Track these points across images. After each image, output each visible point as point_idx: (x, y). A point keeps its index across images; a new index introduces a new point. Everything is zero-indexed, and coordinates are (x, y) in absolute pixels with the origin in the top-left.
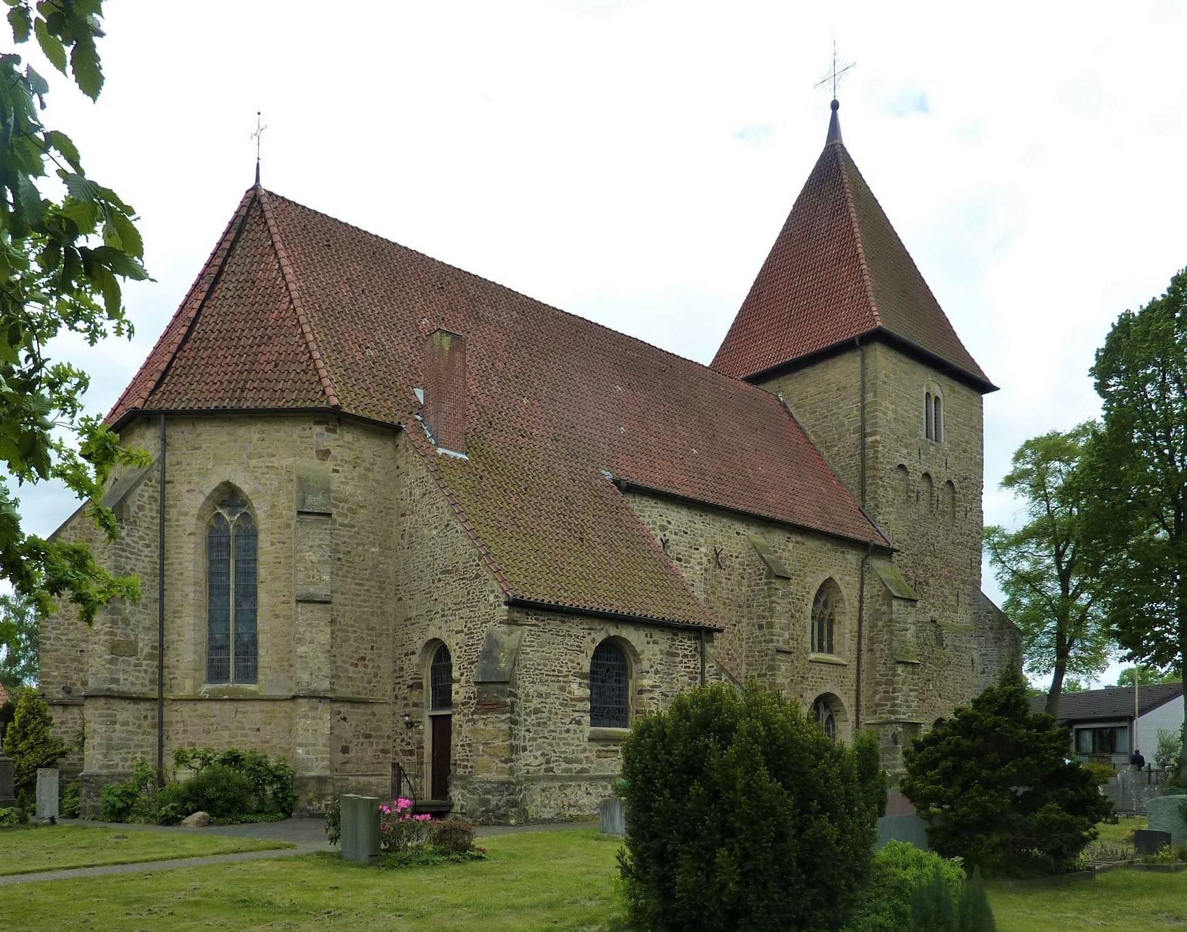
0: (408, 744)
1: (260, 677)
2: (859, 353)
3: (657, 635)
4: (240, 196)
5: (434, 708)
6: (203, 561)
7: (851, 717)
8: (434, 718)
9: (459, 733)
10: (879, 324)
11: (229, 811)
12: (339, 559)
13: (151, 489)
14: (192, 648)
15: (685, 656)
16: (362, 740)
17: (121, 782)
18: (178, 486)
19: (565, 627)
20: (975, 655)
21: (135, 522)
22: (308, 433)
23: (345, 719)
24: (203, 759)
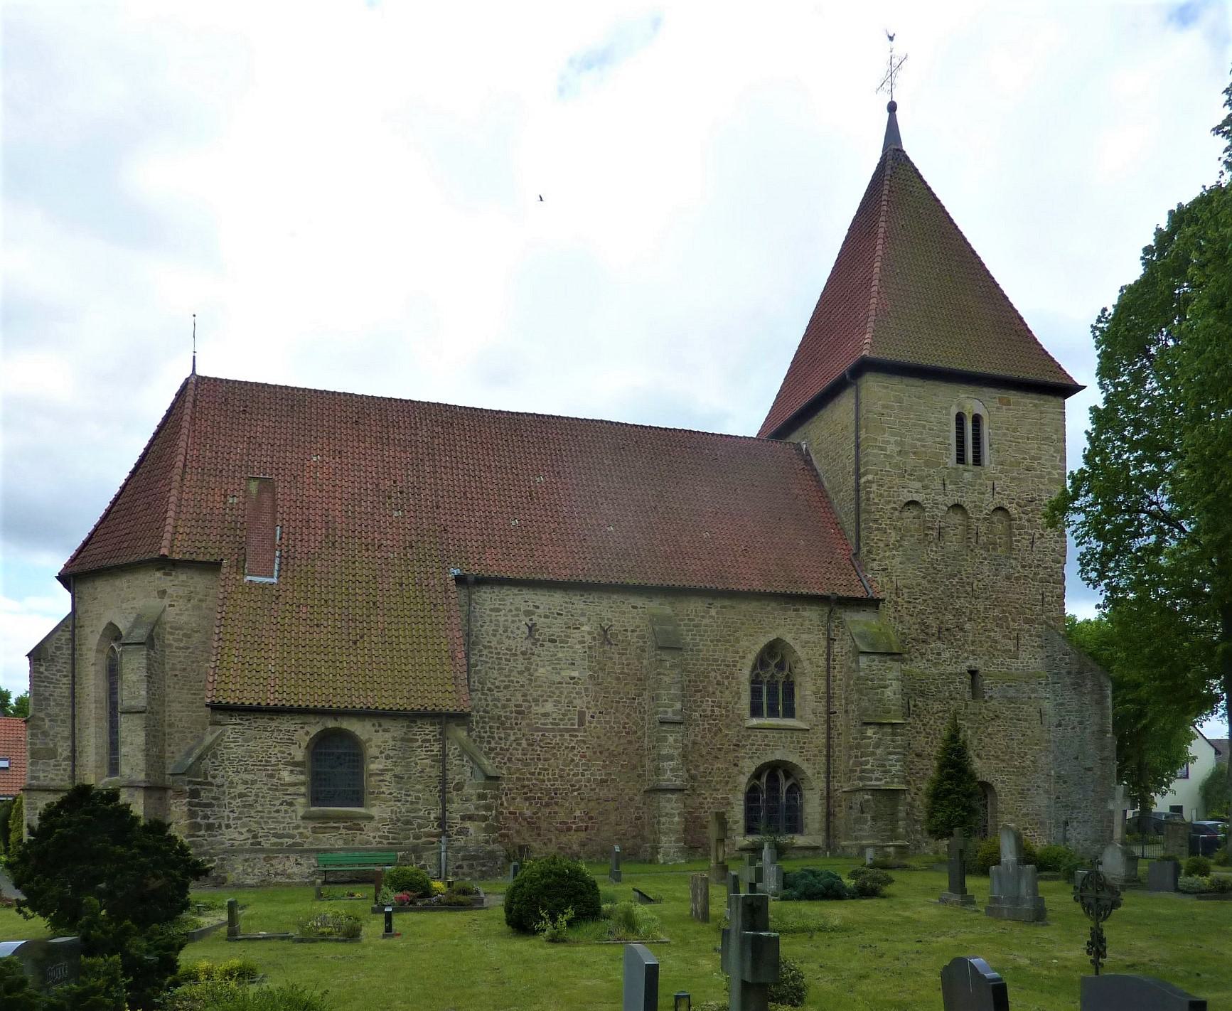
3: (387, 724)
19: (273, 724)
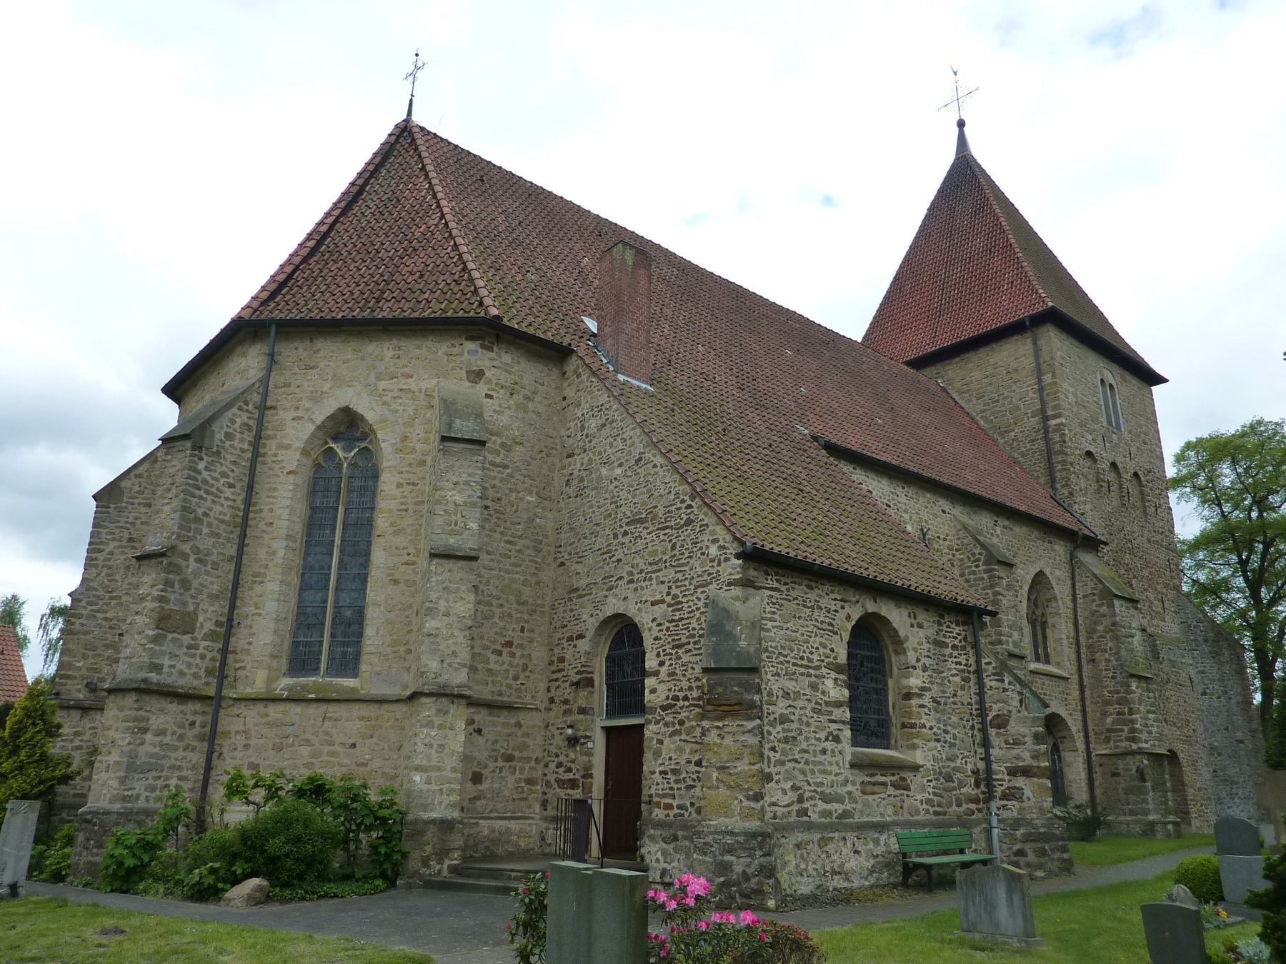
0: (569, 770)
1: (364, 667)
2: (1029, 334)
3: (922, 617)
4: (389, 128)
5: (609, 715)
6: (302, 509)
7: (1081, 745)
8: (608, 730)
9: (657, 753)
12: (491, 507)
14: (272, 625)
15: (955, 647)
16: (500, 763)
18: (281, 412)
19: (813, 596)
20: (1193, 672)
21: (218, 453)
22: (456, 350)
23: (479, 731)
24: (269, 788)
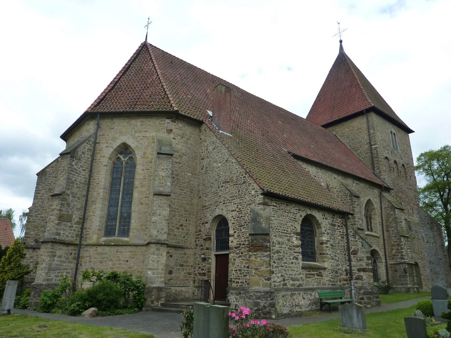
0: (203, 270)
1: (131, 234)
2: (365, 115)
3: (327, 215)
6: (109, 178)
7: (384, 260)
8: (216, 256)
9: (234, 264)
10: (373, 105)
11: (109, 307)
12: (175, 177)
13: (89, 145)
14: (99, 219)
15: (339, 226)
16: (179, 267)
17: (53, 289)
18: (101, 144)
19: (288, 208)
20: (423, 235)
21: (80, 159)
23: (171, 256)
24: (98, 276)
